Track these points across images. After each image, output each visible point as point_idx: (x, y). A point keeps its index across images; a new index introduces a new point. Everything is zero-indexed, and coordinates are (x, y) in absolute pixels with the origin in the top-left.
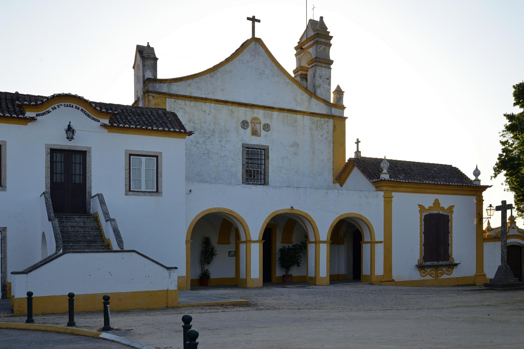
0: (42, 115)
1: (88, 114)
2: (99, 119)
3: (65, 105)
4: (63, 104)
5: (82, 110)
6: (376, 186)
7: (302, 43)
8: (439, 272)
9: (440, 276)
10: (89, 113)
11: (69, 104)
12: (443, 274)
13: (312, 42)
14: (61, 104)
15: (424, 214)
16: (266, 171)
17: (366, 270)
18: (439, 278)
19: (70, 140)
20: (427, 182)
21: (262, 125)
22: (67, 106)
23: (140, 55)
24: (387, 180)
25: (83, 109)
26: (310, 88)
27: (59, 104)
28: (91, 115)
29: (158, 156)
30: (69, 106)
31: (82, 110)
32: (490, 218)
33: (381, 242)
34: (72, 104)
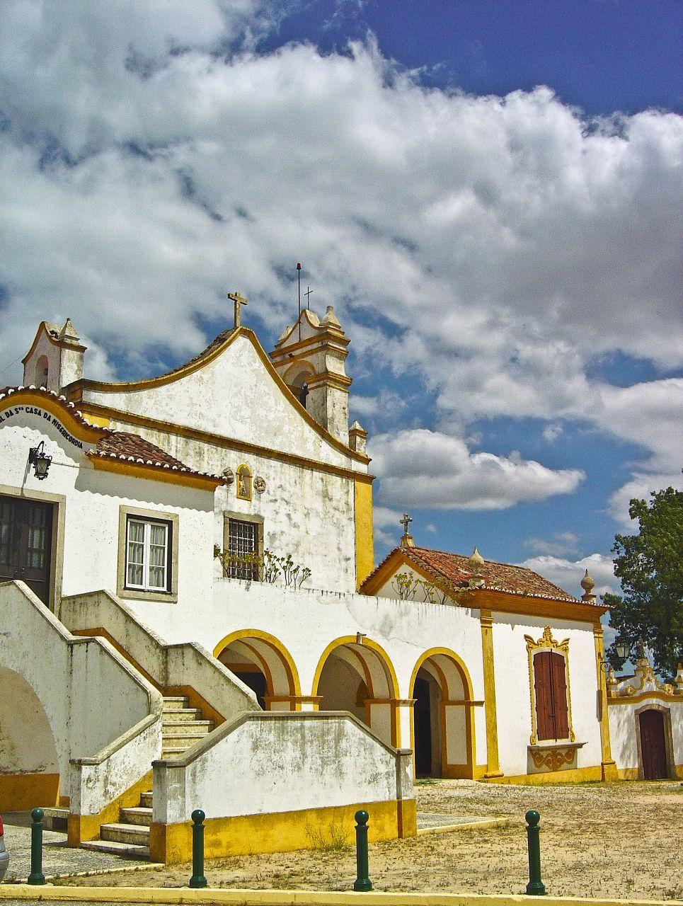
0: (61, 431)
3: (28, 410)
4: (25, 406)
5: (54, 421)
10: (65, 429)
11: (34, 407)
14: (21, 406)
15: (534, 652)
17: (454, 756)
19: (40, 479)
20: (540, 595)
21: (253, 480)
22: (31, 412)
23: (491, 418)
25: (57, 419)
27: (18, 406)
28: (69, 433)
30: (34, 411)
31: (54, 421)
33: (480, 704)
34: (39, 409)
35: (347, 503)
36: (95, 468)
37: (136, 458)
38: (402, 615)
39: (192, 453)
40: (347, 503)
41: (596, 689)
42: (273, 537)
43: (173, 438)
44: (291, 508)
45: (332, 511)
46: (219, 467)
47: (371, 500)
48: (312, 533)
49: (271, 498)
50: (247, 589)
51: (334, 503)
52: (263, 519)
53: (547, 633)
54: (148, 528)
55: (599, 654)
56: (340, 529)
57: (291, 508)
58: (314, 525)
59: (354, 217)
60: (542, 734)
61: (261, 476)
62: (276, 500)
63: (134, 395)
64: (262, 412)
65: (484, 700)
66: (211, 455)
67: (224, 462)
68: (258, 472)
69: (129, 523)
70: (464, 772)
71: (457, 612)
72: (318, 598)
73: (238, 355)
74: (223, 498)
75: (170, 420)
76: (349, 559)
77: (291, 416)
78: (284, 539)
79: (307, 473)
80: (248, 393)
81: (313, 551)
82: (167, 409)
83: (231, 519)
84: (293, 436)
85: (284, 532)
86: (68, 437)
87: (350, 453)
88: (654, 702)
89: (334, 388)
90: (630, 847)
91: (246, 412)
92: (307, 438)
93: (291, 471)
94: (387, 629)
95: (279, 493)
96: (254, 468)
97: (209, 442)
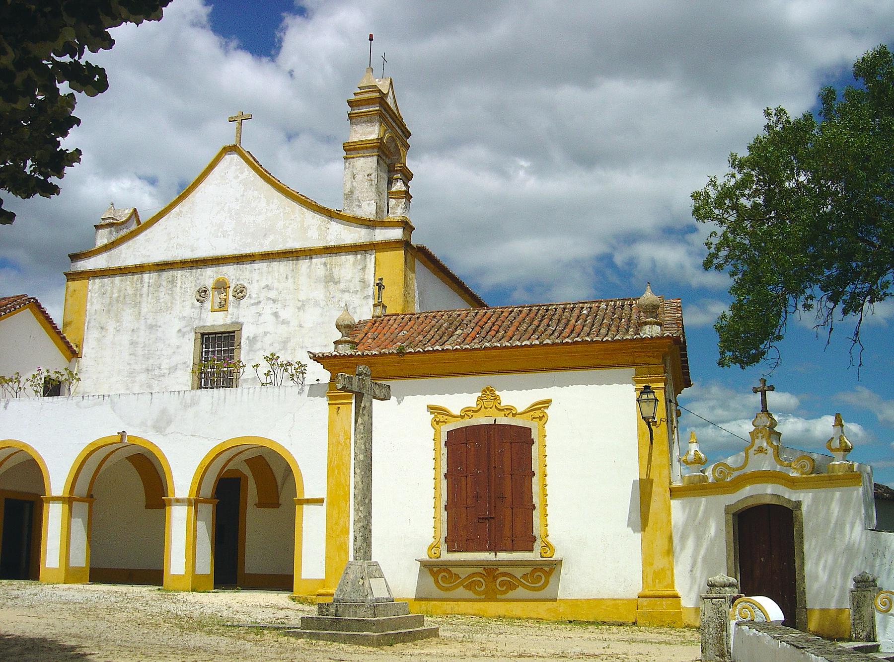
12: (515, 587)
17: (875, 640)
20: (488, 345)
33: (320, 501)
35: (363, 281)
38: (186, 407)
39: (164, 283)
40: (363, 281)
41: (634, 474)
42: (253, 340)
44: (279, 305)
45: (338, 295)
49: (253, 301)
50: (495, 421)
51: (342, 286)
53: (489, 394)
59: (277, 66)
60: (454, 541)
61: (241, 282)
62: (259, 302)
63: (115, 252)
72: (77, 404)
77: (288, 210)
78: (268, 339)
85: (268, 332)
89: (353, 158)
90: (244, 613)
92: (308, 227)
93: (281, 267)
95: (264, 294)
97: (183, 268)
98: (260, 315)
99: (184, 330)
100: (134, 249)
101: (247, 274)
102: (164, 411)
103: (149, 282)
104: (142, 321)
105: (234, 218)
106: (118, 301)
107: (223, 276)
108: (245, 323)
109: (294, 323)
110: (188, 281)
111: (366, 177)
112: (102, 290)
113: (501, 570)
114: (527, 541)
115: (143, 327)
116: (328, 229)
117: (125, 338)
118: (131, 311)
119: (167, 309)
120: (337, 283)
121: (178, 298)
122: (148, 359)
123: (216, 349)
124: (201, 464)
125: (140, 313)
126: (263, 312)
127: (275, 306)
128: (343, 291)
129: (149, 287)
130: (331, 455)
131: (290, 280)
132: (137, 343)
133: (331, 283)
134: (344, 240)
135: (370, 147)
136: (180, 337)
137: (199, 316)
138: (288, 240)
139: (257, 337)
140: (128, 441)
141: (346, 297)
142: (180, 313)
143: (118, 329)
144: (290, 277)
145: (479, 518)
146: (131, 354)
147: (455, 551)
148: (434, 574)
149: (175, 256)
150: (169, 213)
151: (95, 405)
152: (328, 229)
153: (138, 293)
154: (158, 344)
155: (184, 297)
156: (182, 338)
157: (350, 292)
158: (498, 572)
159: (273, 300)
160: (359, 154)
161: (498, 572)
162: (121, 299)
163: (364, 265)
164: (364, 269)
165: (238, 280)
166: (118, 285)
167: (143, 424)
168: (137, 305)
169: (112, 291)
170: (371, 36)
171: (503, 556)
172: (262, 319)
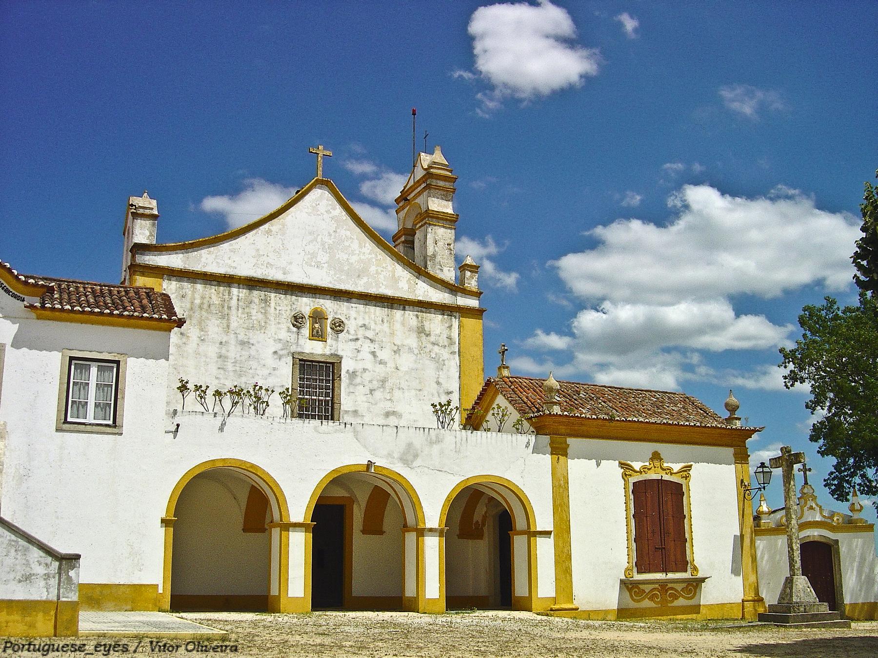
1: (7, 288)
2: (23, 296)
6: (536, 426)
7: (407, 191)
8: (670, 592)
9: (672, 602)
10: (8, 287)
12: (676, 598)
13: (423, 185)
16: (336, 401)
17: (520, 589)
18: (669, 605)
20: (635, 419)
21: (329, 321)
24: (555, 414)
26: (418, 261)
28: (11, 290)
29: (120, 361)
32: (764, 488)
33: (547, 534)
35: (449, 338)
36: (38, 319)
37: (73, 307)
39: (257, 300)
40: (449, 338)
43: (235, 291)
44: (376, 346)
45: (430, 346)
46: (289, 311)
47: (481, 332)
48: (403, 369)
49: (351, 337)
51: (432, 338)
52: (341, 358)
53: (656, 457)
54: (94, 370)
55: (742, 481)
56: (440, 364)
57: (376, 346)
58: (406, 361)
60: (642, 565)
61: (339, 317)
62: (357, 339)
64: (342, 256)
65: (552, 529)
66: (280, 301)
67: (294, 307)
68: (336, 313)
69: (73, 367)
70: (524, 605)
71: (514, 441)
73: (314, 205)
74: (292, 341)
75: (231, 272)
76: (451, 393)
77: (379, 257)
78: (367, 376)
79: (398, 314)
80: (326, 239)
81: (404, 384)
82: (229, 262)
83: (300, 360)
84: (381, 276)
85: (367, 369)
86: (11, 294)
87: (455, 289)
88: (814, 533)
89: (435, 225)
91: (323, 257)
93: (377, 312)
94: (410, 458)
95: (361, 333)
96: (330, 310)
98: (358, 351)
99: (281, 353)
100: (216, 256)
101: (353, 314)
102: (410, 445)
103: (238, 296)
104: (232, 336)
105: (328, 251)
106: (201, 307)
107: (320, 307)
108: (344, 357)
109: (391, 365)
110: (283, 305)
111: (446, 245)
112: (181, 292)
113: (670, 585)
114: (682, 564)
115: (233, 342)
116: (417, 284)
117: (212, 350)
118: (218, 321)
119: (261, 327)
120: (428, 335)
121: (272, 319)
122: (240, 376)
123: (325, 378)
124: (448, 497)
125: (228, 326)
126: (361, 349)
127: (372, 345)
128: (434, 344)
129: (238, 300)
130: (555, 495)
131: (386, 324)
132: (226, 357)
133: (423, 335)
134: (430, 298)
135: (449, 220)
136: (277, 359)
137: (296, 342)
138: (381, 285)
139: (357, 372)
140: (374, 470)
141: (436, 349)
142: (275, 334)
143: (202, 338)
144: (385, 321)
145: (656, 548)
146: (219, 368)
147: (642, 572)
148: (630, 590)
149: (265, 274)
150: (258, 229)
151: (336, 431)
152: (417, 284)
153: (226, 305)
154: (251, 363)
155: (279, 319)
156: (278, 360)
157: (439, 346)
158: (667, 587)
159: (370, 340)
160: (439, 222)
161: (667, 587)
162: (205, 306)
163: (450, 324)
164: (450, 327)
165: (336, 313)
166: (201, 291)
167: (390, 455)
168: (225, 317)
169: (193, 295)
170: (414, 111)
171: (671, 576)
172: (360, 356)
